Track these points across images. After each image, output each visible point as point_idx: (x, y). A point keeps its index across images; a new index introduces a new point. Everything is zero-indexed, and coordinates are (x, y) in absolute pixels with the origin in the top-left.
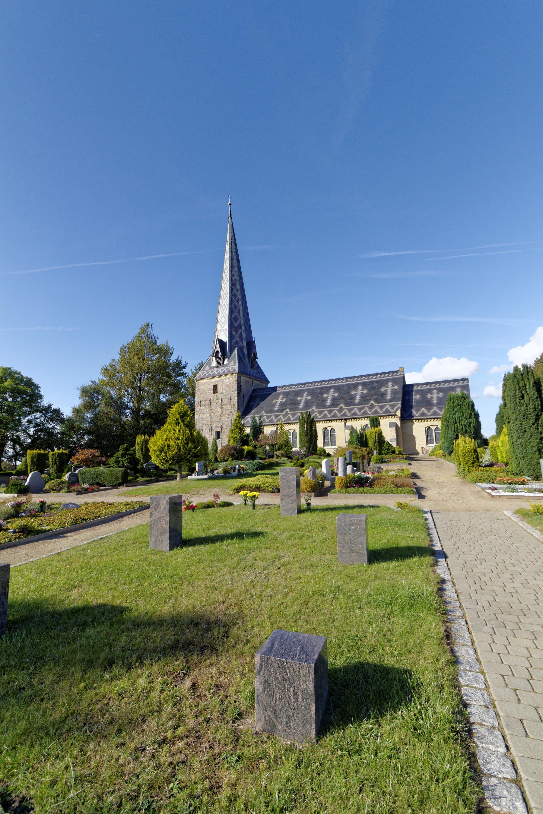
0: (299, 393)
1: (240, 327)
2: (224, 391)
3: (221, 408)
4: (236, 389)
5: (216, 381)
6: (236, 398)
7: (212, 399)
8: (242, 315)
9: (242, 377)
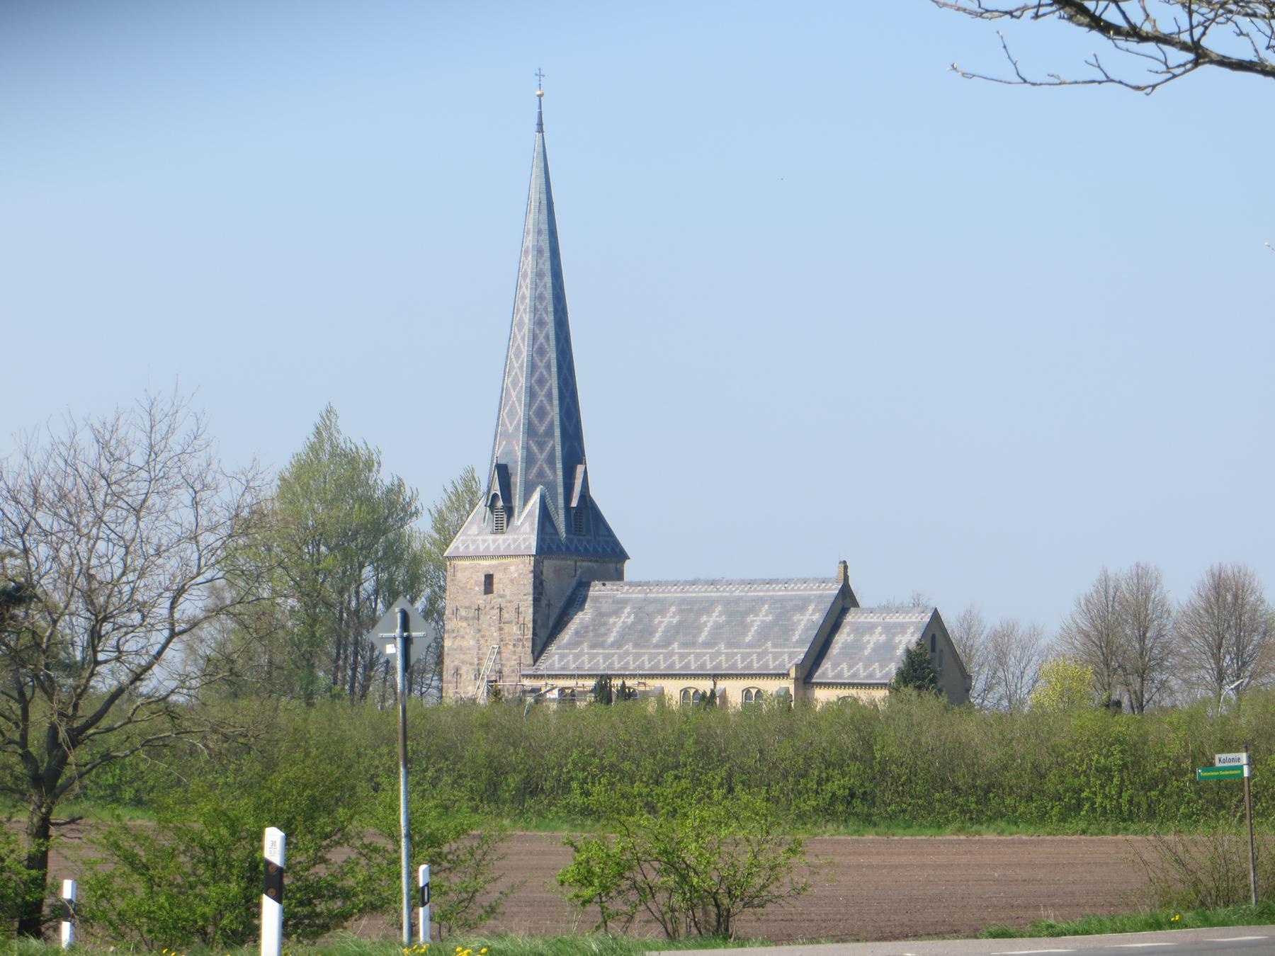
0: (706, 607)
1: (549, 432)
2: (508, 593)
3: (501, 629)
4: (530, 589)
5: (490, 566)
6: (531, 610)
7: (482, 606)
8: (556, 402)
9: (546, 563)
